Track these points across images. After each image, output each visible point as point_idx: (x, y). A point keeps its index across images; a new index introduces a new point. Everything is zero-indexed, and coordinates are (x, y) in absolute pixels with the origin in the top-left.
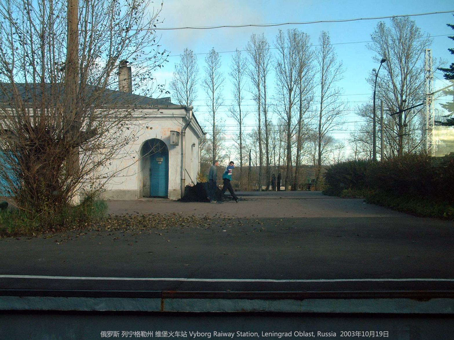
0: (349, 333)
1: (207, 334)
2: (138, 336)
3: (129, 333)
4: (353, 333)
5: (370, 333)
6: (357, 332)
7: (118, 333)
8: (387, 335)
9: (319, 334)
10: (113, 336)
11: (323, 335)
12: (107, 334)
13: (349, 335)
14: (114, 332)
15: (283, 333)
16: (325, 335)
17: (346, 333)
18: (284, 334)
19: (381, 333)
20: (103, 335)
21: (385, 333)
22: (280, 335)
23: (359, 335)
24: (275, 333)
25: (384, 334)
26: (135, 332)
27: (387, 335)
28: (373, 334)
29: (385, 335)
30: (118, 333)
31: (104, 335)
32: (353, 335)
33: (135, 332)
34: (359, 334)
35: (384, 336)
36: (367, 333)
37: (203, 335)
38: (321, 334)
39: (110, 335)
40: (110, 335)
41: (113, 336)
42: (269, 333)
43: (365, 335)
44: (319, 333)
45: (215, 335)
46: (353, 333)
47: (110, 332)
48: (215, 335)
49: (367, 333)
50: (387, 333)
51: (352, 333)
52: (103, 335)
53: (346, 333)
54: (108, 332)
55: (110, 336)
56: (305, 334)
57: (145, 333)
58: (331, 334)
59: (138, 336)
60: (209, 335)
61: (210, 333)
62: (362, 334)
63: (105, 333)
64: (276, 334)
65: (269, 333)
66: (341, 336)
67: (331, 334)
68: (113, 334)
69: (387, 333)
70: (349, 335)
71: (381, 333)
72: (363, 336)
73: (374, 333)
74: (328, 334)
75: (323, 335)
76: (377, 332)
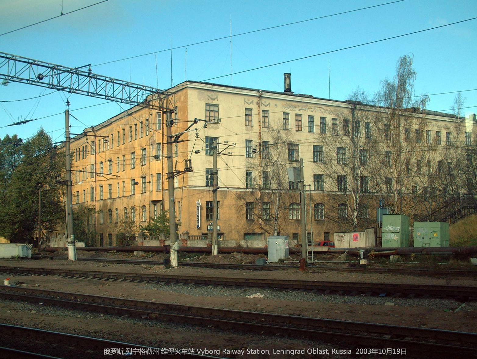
0: (365, 350)
1: (215, 352)
2: (143, 353)
3: (134, 350)
4: (369, 350)
5: (387, 350)
6: (373, 349)
7: (122, 350)
8: (405, 353)
9: (334, 351)
10: (116, 353)
11: (338, 352)
12: (111, 351)
13: (365, 352)
14: (118, 349)
15: (295, 351)
16: (340, 352)
17: (361, 350)
18: (297, 352)
19: (398, 350)
20: (106, 352)
21: (403, 350)
22: (292, 352)
23: (375, 353)
24: (287, 351)
25: (402, 351)
26: (140, 350)
27: (405, 353)
28: (390, 351)
29: (403, 353)
30: (122, 350)
31: (107, 353)
32: (369, 352)
33: (140, 350)
34: (376, 352)
35: (402, 354)
36: (384, 350)
37: (211, 352)
38: (335, 351)
39: (114, 353)
40: (114, 353)
41: (116, 353)
42: (266, 351)
43: (381, 352)
44: (334, 350)
45: (333, 352)
46: (369, 350)
47: (114, 350)
48: (333, 352)
49: (384, 350)
50: (405, 350)
51: (368, 350)
52: (106, 352)
53: (361, 350)
54: (112, 350)
55: (113, 354)
56: (319, 352)
57: (150, 350)
58: (346, 351)
59: (143, 353)
60: (218, 352)
61: (219, 351)
62: (378, 351)
63: (108, 350)
64: (288, 351)
65: (281, 351)
66: (357, 353)
67: (346, 351)
68: (117, 351)
69: (405, 350)
70: (365, 352)
71: (398, 350)
72: (380, 353)
73: (391, 350)
74: (343, 351)
75: (338, 352)
76: (395, 349)
